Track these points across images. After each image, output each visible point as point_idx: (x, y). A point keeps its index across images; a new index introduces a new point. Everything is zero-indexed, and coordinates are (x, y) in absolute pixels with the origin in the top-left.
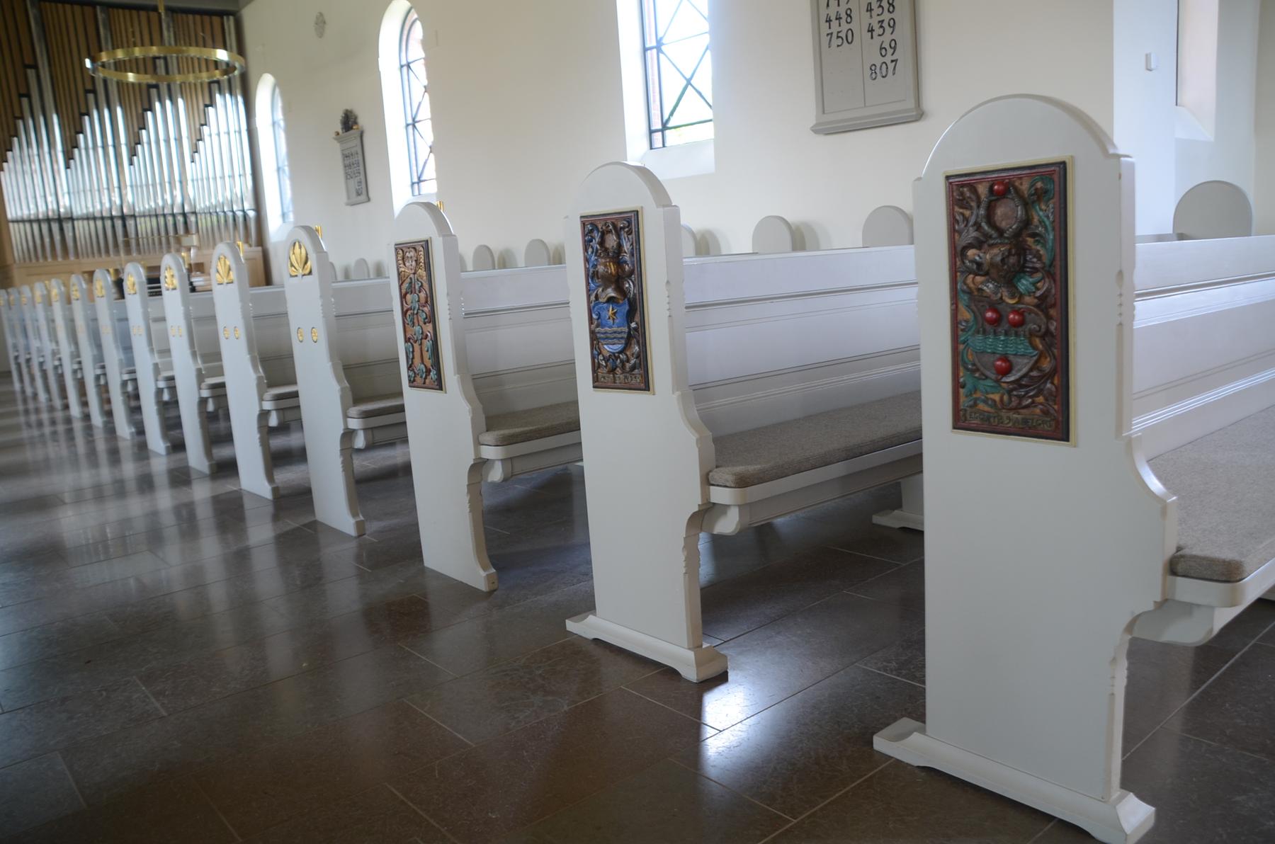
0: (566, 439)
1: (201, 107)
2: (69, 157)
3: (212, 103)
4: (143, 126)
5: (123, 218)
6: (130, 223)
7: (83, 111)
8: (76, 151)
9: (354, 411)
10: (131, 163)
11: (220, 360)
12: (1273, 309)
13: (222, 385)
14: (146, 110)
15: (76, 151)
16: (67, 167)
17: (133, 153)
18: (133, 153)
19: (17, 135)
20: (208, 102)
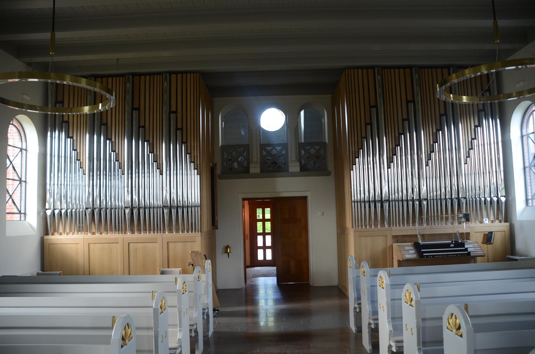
0: (83, 90)
1: (473, 127)
2: (390, 161)
3: (480, 125)
4: (436, 141)
5: (382, 202)
6: (386, 205)
7: (401, 132)
8: (354, 166)
9: (392, 339)
10: (427, 165)
11: (442, 345)
12: (534, 303)
13: (402, 342)
14: (356, 158)
15: (354, 166)
16: (389, 167)
17: (429, 158)
18: (429, 158)
19: (362, 148)
20: (477, 124)
